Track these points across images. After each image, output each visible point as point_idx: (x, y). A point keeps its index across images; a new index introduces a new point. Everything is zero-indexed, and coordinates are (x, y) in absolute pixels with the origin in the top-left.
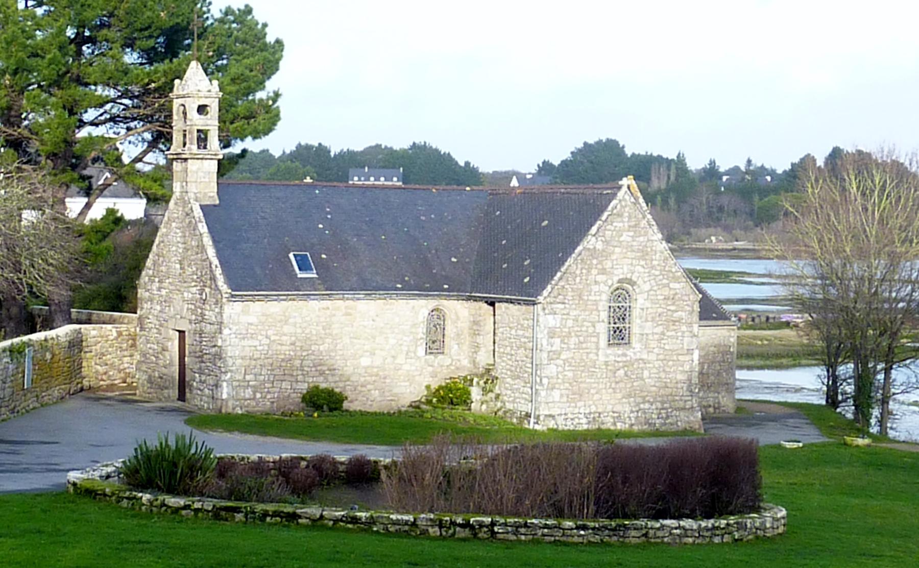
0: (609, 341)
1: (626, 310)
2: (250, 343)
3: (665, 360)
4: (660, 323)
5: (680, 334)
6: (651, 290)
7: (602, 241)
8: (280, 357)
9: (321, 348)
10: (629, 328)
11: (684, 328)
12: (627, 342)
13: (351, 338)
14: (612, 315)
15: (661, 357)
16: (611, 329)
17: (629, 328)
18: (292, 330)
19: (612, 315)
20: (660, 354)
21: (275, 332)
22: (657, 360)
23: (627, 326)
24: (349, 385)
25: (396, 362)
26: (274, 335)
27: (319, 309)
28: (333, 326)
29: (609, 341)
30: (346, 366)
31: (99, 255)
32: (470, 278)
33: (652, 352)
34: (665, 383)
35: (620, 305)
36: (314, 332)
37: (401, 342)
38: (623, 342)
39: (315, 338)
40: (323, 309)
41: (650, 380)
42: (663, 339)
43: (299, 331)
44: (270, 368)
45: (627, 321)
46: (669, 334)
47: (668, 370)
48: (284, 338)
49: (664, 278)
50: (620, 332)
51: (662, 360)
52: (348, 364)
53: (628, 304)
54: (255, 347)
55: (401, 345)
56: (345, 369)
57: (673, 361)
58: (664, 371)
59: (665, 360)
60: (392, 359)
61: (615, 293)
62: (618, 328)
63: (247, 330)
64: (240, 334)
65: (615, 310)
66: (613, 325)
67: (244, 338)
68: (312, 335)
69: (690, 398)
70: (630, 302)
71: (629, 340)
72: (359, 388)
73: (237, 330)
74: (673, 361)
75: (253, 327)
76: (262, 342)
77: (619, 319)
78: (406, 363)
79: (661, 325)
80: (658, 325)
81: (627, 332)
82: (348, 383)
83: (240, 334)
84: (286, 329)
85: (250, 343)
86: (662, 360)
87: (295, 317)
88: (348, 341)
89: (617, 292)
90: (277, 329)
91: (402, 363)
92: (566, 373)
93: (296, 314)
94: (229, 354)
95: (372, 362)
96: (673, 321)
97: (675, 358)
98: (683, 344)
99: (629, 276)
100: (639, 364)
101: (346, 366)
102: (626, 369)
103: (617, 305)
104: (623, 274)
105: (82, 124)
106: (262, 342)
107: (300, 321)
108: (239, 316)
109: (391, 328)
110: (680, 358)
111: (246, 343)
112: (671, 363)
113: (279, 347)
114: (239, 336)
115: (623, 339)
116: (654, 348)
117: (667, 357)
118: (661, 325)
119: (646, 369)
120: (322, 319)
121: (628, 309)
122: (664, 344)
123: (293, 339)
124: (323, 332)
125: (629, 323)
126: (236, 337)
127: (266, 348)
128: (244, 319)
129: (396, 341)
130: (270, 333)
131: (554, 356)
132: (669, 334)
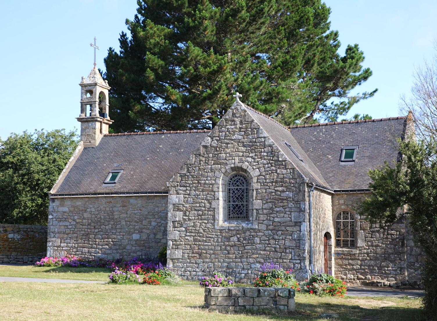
0: (229, 215)
1: (243, 191)
2: (64, 224)
3: (274, 230)
4: (269, 200)
5: (287, 209)
6: (260, 175)
7: (217, 140)
8: (81, 232)
9: (107, 227)
10: (247, 205)
11: (291, 205)
12: (245, 215)
13: (126, 221)
14: (231, 195)
15: (271, 227)
16: (231, 206)
17: (247, 205)
18: (89, 216)
19: (231, 195)
20: (270, 225)
21: (79, 217)
22: (267, 230)
23: (245, 203)
24: (125, 252)
25: (156, 237)
26: (78, 219)
27: (105, 203)
28: (114, 214)
29: (229, 215)
30: (123, 239)
31: (302, 211)
32: (60, 163)
33: (263, 223)
34: (275, 248)
35: (238, 188)
36: (102, 217)
37: (160, 224)
38: (242, 216)
39: (103, 221)
40: (108, 202)
41: (261, 246)
42: (272, 214)
43: (93, 216)
44: (75, 239)
45: (245, 200)
46: (278, 209)
47: (276, 237)
48: (84, 221)
49: (272, 166)
50: (239, 208)
51: (271, 230)
52: (124, 238)
53: (245, 187)
54: (67, 226)
55: (160, 226)
56: (122, 241)
57: (282, 231)
58: (273, 239)
59: (274, 230)
60: (154, 235)
61: (233, 179)
62: (237, 205)
63: (63, 216)
64: (58, 218)
65: (234, 192)
66: (232, 203)
67: (60, 221)
68: (101, 219)
69: (298, 261)
70: (247, 185)
71: (247, 215)
72: (132, 254)
73: (56, 216)
74: (282, 231)
75: (66, 214)
76: (71, 224)
77: (237, 198)
78: (163, 238)
79: (270, 202)
80: (267, 202)
81: (245, 208)
82: (124, 250)
83: (58, 218)
84: (86, 215)
85: (64, 224)
86: (271, 230)
87: (91, 208)
88: (124, 223)
89: (236, 178)
90: (80, 215)
91: (161, 238)
92: (186, 237)
93: (91, 206)
94: (52, 231)
95: (140, 237)
96: (281, 199)
97: (283, 228)
98: (291, 218)
99: (239, 165)
100: (251, 232)
101: (123, 239)
102: (238, 236)
103: (236, 188)
104: (234, 164)
105: (113, 122)
106: (71, 224)
107: (94, 211)
108: (58, 208)
109: (153, 215)
110: (288, 228)
111: (61, 224)
112: (280, 232)
113: (81, 226)
114: (58, 220)
115: (241, 213)
116: (264, 221)
117: (276, 228)
118: (270, 202)
119: (257, 237)
120: (108, 209)
121: (245, 191)
122: (274, 218)
123: (90, 221)
124: (108, 217)
125: (247, 201)
126: (56, 220)
127: (74, 227)
128: (61, 209)
129: (156, 223)
130: (76, 217)
131: (177, 224)
132: (278, 209)
